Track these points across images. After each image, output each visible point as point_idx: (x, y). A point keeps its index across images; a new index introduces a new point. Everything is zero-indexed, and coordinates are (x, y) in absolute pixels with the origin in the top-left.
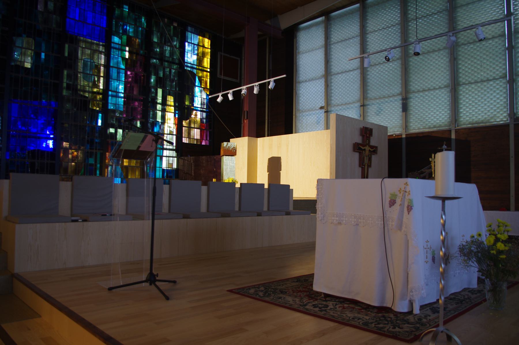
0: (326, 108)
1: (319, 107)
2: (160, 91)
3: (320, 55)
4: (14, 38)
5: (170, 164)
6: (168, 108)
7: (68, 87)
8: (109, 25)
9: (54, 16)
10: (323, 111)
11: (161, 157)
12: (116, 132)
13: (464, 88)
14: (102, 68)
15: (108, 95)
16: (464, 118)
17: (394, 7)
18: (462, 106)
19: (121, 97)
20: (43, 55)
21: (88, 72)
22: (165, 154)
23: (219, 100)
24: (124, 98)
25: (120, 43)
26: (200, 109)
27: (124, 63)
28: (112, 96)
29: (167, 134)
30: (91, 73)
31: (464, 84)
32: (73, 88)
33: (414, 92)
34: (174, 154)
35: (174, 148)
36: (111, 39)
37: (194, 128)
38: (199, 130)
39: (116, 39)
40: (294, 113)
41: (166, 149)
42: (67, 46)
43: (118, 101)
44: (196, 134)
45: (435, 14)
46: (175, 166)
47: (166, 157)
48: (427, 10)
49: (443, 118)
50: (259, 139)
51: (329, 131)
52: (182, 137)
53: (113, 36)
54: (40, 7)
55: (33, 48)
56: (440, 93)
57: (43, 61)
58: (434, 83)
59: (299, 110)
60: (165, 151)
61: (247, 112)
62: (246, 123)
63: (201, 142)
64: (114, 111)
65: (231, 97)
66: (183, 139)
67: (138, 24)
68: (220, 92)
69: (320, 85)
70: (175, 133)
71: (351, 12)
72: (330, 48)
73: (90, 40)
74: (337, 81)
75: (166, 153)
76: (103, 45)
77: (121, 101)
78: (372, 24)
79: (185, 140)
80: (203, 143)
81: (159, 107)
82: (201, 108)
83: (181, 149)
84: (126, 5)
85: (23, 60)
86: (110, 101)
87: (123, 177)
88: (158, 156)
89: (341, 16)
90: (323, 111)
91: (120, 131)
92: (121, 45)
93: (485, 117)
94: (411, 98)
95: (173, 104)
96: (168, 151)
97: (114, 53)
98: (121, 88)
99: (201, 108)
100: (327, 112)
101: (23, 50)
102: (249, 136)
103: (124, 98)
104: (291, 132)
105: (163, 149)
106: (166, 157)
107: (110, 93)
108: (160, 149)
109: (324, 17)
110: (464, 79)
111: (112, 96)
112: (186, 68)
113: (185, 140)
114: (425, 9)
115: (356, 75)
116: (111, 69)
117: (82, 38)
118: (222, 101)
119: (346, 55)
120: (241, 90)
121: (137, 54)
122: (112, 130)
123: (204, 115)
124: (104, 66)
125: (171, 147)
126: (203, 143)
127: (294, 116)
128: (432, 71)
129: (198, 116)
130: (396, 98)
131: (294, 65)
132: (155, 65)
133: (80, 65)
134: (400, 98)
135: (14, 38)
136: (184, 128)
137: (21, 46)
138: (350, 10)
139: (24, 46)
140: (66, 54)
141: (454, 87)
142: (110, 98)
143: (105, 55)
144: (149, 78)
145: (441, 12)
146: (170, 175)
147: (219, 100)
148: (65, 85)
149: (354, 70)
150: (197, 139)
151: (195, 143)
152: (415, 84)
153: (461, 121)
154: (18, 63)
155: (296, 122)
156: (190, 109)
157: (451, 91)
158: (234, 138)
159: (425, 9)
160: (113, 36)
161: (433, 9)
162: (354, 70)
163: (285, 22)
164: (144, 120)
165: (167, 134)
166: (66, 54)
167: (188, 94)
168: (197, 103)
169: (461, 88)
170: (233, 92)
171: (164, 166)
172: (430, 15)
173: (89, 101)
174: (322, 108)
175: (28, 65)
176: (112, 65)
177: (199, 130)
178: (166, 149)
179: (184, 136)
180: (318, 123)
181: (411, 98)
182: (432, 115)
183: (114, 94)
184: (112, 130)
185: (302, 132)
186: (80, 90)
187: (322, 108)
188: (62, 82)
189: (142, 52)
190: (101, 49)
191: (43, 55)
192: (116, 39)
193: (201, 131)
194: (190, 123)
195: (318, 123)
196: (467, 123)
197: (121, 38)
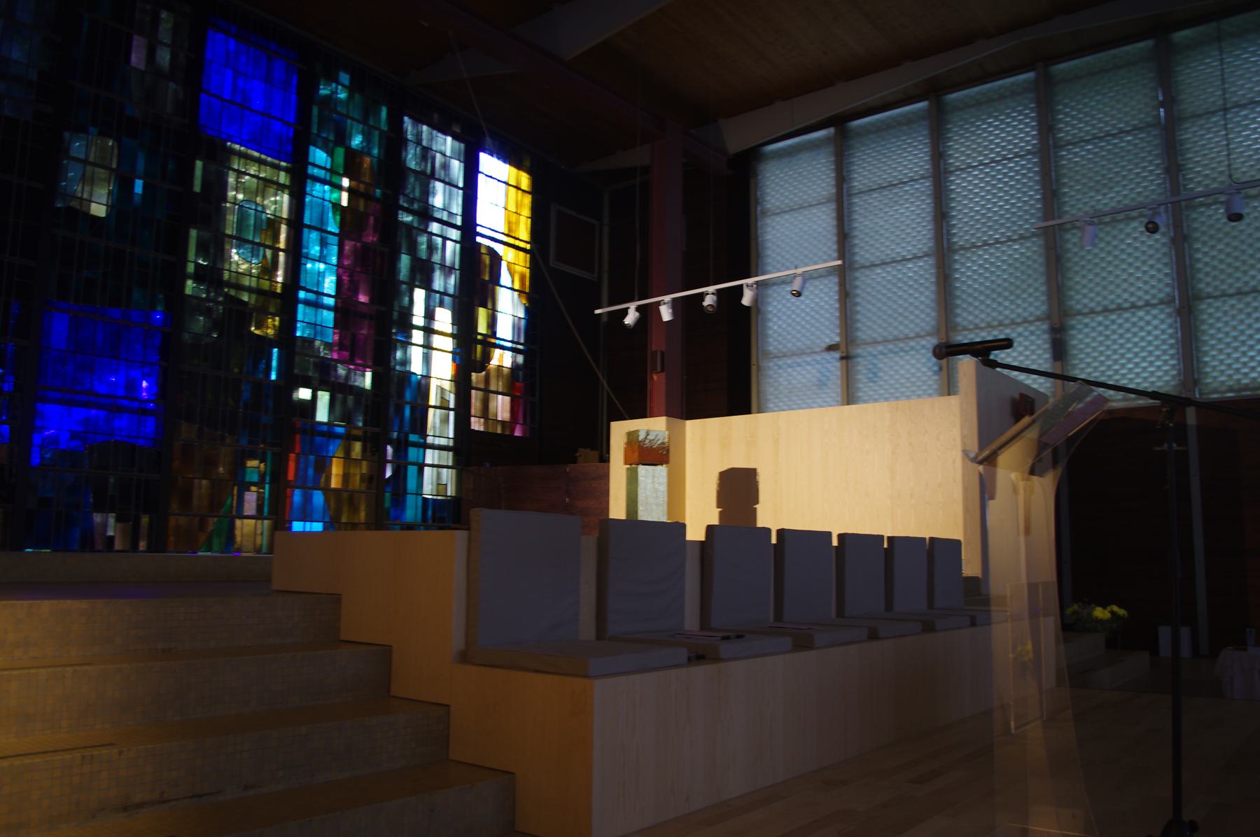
0: (843, 347)
1: (824, 345)
2: (419, 295)
3: (823, 221)
4: (67, 135)
5: (440, 486)
6: (437, 341)
7: (200, 275)
8: (303, 117)
9: (172, 86)
10: (837, 355)
11: (421, 467)
12: (314, 397)
13: (1210, 305)
14: (284, 228)
15: (297, 301)
16: (1215, 378)
17: (1020, 113)
18: (1206, 348)
19: (328, 308)
20: (139, 186)
21: (250, 238)
22: (428, 461)
23: (630, 319)
24: (334, 309)
25: (328, 166)
26: (509, 345)
27: (338, 218)
28: (307, 303)
29: (435, 407)
30: (257, 240)
31: (1209, 296)
32: (212, 276)
33: (1079, 313)
34: (448, 458)
35: (451, 444)
36: (307, 153)
37: (498, 393)
38: (508, 399)
39: (319, 156)
40: (753, 360)
41: (433, 447)
42: (199, 164)
43: (316, 322)
44: (501, 406)
45: (1128, 133)
46: (450, 491)
47: (432, 466)
48: (1106, 123)
49: (1159, 377)
50: (689, 423)
51: (954, 401)
52: (469, 416)
53: (312, 148)
54: (137, 59)
55: (114, 166)
56: (1148, 318)
57: (137, 199)
58: (1092, 300)
59: (767, 354)
60: (429, 452)
61: (662, 353)
62: (658, 381)
63: (513, 431)
64: (308, 342)
65: (666, 314)
66: (473, 419)
67: (371, 123)
68: (631, 300)
69: (824, 296)
70: (452, 405)
71: (909, 121)
72: (851, 204)
73: (256, 154)
74: (869, 284)
75: (431, 456)
76: (286, 170)
77: (328, 317)
78: (960, 150)
79: (477, 424)
80: (517, 433)
81: (418, 337)
82: (511, 342)
83: (467, 448)
84: (346, 71)
85: (86, 196)
86: (300, 317)
87: (327, 519)
88: (413, 464)
89: (878, 129)
90: (837, 355)
91: (324, 398)
92: (332, 171)
93: (1235, 377)
94: (1073, 327)
95: (449, 329)
96: (436, 452)
97: (318, 190)
98: (329, 285)
99: (511, 342)
100: (846, 358)
101: (89, 169)
102: (669, 414)
103: (334, 309)
104: (746, 410)
105: (426, 446)
106: (432, 466)
107: (302, 294)
108: (415, 445)
109: (831, 130)
110: (1208, 284)
111: (307, 303)
112: (479, 239)
113: (477, 424)
114: (1100, 120)
115: (924, 271)
116: (306, 231)
117: (237, 147)
118: (639, 322)
119: (895, 223)
120: (701, 296)
121: (368, 197)
122: (304, 394)
123: (520, 359)
124: (289, 222)
125: (443, 442)
126: (517, 433)
127: (754, 369)
128: (1125, 268)
129: (502, 359)
130: (1032, 328)
131: (753, 243)
132: (409, 226)
133: (232, 219)
134: (1045, 327)
135: (67, 135)
136: (473, 392)
137: (82, 156)
138: (882, 121)
139: (91, 159)
140: (197, 188)
141: (1186, 306)
142: (301, 307)
143: (291, 195)
144: (395, 260)
145: (1140, 129)
146: (445, 514)
147: (630, 319)
148: (191, 268)
149: (916, 257)
150: (503, 422)
151: (499, 431)
152: (1083, 294)
153: (1207, 384)
154: (75, 204)
155: (758, 383)
156: (490, 342)
157: (1179, 312)
158: (625, 419)
159: (1100, 120)
160: (312, 148)
161: (1120, 120)
162: (916, 257)
163: (735, 137)
164: (380, 369)
165: (435, 407)
166: (197, 188)
167: (485, 306)
168: (505, 330)
169: (1203, 306)
170: (674, 300)
171: (428, 490)
172: (1114, 136)
173: (251, 314)
174: (831, 348)
175: (99, 210)
176: (307, 221)
177: (508, 399)
178: (433, 447)
179: (473, 412)
180: (821, 384)
181: (1073, 327)
182: (1130, 369)
183: (311, 296)
184: (304, 394)
185: (865, 402)
186: (229, 284)
187: (831, 348)
188: (185, 261)
189: (378, 192)
190: (283, 178)
191: (139, 186)
192: (319, 156)
193: (512, 401)
194: (487, 380)
195: (821, 384)
196: (1224, 388)
197: (331, 154)
